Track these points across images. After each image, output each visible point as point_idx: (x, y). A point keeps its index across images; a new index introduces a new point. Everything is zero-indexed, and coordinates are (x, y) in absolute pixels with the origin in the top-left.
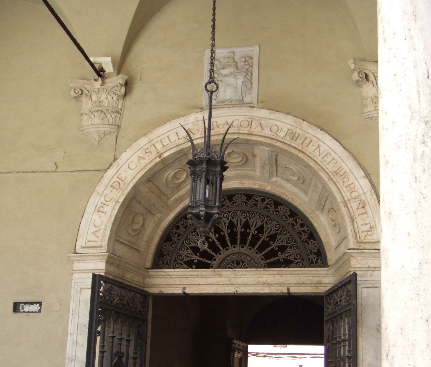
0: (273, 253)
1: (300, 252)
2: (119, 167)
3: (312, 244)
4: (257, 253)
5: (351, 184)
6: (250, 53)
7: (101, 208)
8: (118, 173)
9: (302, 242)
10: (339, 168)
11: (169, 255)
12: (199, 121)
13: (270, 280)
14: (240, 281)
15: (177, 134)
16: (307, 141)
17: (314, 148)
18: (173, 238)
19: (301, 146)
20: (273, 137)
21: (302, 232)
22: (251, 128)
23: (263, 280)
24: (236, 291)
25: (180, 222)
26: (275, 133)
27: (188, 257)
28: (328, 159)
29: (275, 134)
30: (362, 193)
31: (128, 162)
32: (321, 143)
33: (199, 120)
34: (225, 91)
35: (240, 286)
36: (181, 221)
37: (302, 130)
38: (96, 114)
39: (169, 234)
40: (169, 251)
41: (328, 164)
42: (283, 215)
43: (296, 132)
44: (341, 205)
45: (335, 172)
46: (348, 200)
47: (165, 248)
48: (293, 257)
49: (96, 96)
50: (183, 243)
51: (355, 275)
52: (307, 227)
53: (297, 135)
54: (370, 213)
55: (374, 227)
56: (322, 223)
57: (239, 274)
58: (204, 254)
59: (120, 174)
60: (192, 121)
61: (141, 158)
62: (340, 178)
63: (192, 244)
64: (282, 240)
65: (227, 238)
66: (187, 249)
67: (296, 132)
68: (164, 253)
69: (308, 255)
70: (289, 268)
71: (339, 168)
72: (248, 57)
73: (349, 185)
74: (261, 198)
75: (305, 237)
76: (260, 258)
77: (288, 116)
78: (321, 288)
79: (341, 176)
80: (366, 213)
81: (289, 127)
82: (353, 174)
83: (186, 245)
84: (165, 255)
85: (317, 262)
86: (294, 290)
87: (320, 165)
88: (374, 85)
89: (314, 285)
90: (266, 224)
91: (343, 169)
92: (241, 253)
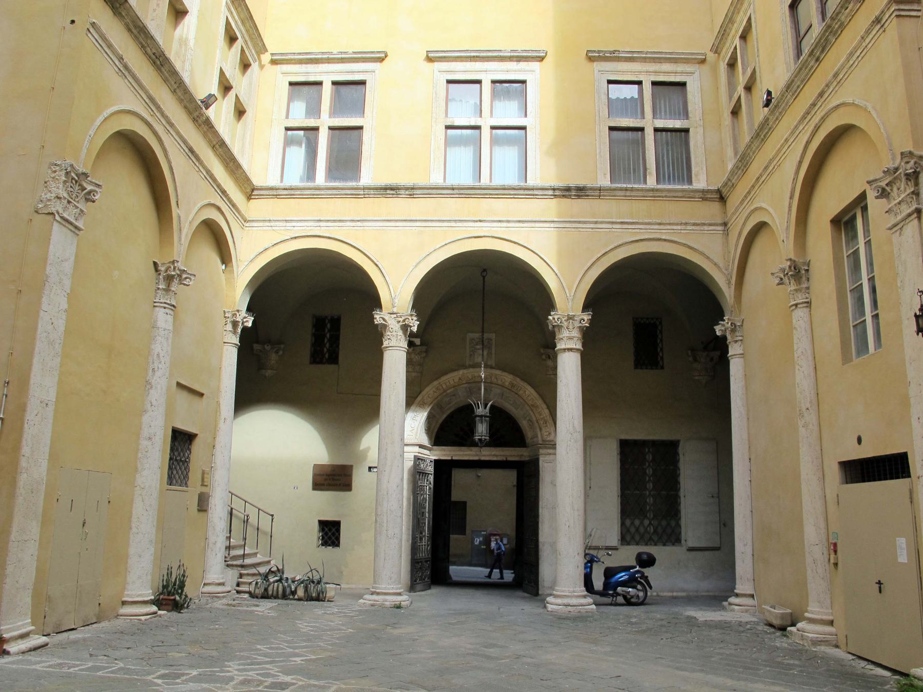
13: (497, 453)
56: (524, 424)
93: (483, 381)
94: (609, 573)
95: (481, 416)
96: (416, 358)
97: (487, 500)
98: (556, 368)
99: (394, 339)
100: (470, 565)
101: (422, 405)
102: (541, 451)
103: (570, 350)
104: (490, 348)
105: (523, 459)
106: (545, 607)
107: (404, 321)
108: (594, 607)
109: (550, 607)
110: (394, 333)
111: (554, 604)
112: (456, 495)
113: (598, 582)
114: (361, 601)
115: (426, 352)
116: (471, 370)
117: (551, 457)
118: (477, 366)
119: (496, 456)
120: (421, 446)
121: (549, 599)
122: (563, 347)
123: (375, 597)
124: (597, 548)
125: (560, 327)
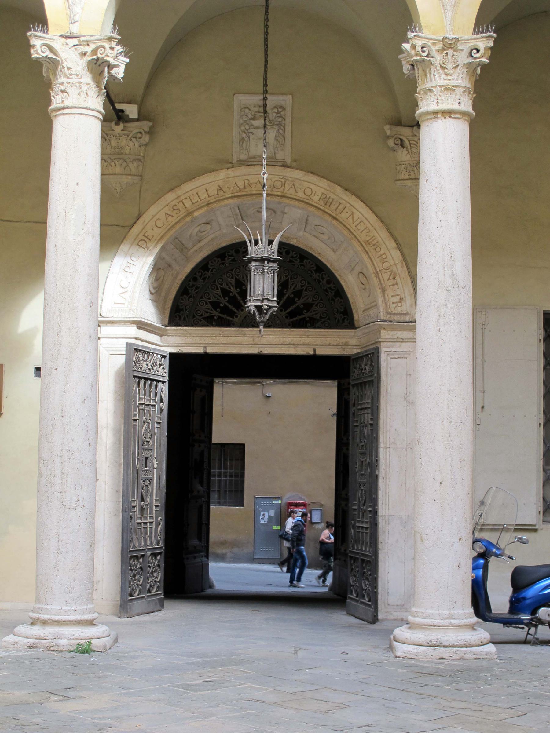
2: (145, 223)
6: (283, 103)
7: (128, 268)
8: (144, 231)
9: (329, 299)
13: (296, 340)
14: (264, 340)
16: (341, 207)
17: (348, 215)
18: (190, 291)
19: (335, 212)
20: (307, 201)
23: (288, 340)
27: (207, 312)
28: (361, 227)
29: (308, 198)
31: (155, 219)
32: (355, 211)
34: (256, 145)
42: (309, 270)
44: (373, 275)
45: (367, 241)
52: (334, 284)
53: (331, 200)
56: (350, 283)
58: (225, 310)
60: (222, 177)
62: (373, 247)
66: (207, 304)
68: (181, 308)
69: (335, 314)
74: (285, 250)
77: (322, 179)
79: (373, 245)
80: (397, 284)
81: (323, 191)
84: (182, 310)
86: (321, 352)
87: (354, 234)
88: (408, 152)
89: (340, 347)
90: (291, 279)
91: (375, 239)
93: (267, 204)
94: (521, 580)
95: (262, 260)
96: (130, 146)
97: (277, 432)
98: (417, 165)
99: (73, 91)
100: (252, 560)
101: (143, 241)
102: (384, 335)
103: (448, 113)
104: (281, 126)
105: (346, 352)
106: (391, 648)
107: (94, 52)
108: (491, 648)
109: (401, 649)
110: (74, 80)
111: (410, 643)
112: (222, 432)
113: (500, 597)
114: (11, 638)
115: (151, 132)
116: (243, 170)
117: (405, 346)
118: (253, 161)
120: (141, 325)
121: (401, 632)
122: (433, 107)
123: (38, 630)
124: (495, 528)
125: (425, 64)
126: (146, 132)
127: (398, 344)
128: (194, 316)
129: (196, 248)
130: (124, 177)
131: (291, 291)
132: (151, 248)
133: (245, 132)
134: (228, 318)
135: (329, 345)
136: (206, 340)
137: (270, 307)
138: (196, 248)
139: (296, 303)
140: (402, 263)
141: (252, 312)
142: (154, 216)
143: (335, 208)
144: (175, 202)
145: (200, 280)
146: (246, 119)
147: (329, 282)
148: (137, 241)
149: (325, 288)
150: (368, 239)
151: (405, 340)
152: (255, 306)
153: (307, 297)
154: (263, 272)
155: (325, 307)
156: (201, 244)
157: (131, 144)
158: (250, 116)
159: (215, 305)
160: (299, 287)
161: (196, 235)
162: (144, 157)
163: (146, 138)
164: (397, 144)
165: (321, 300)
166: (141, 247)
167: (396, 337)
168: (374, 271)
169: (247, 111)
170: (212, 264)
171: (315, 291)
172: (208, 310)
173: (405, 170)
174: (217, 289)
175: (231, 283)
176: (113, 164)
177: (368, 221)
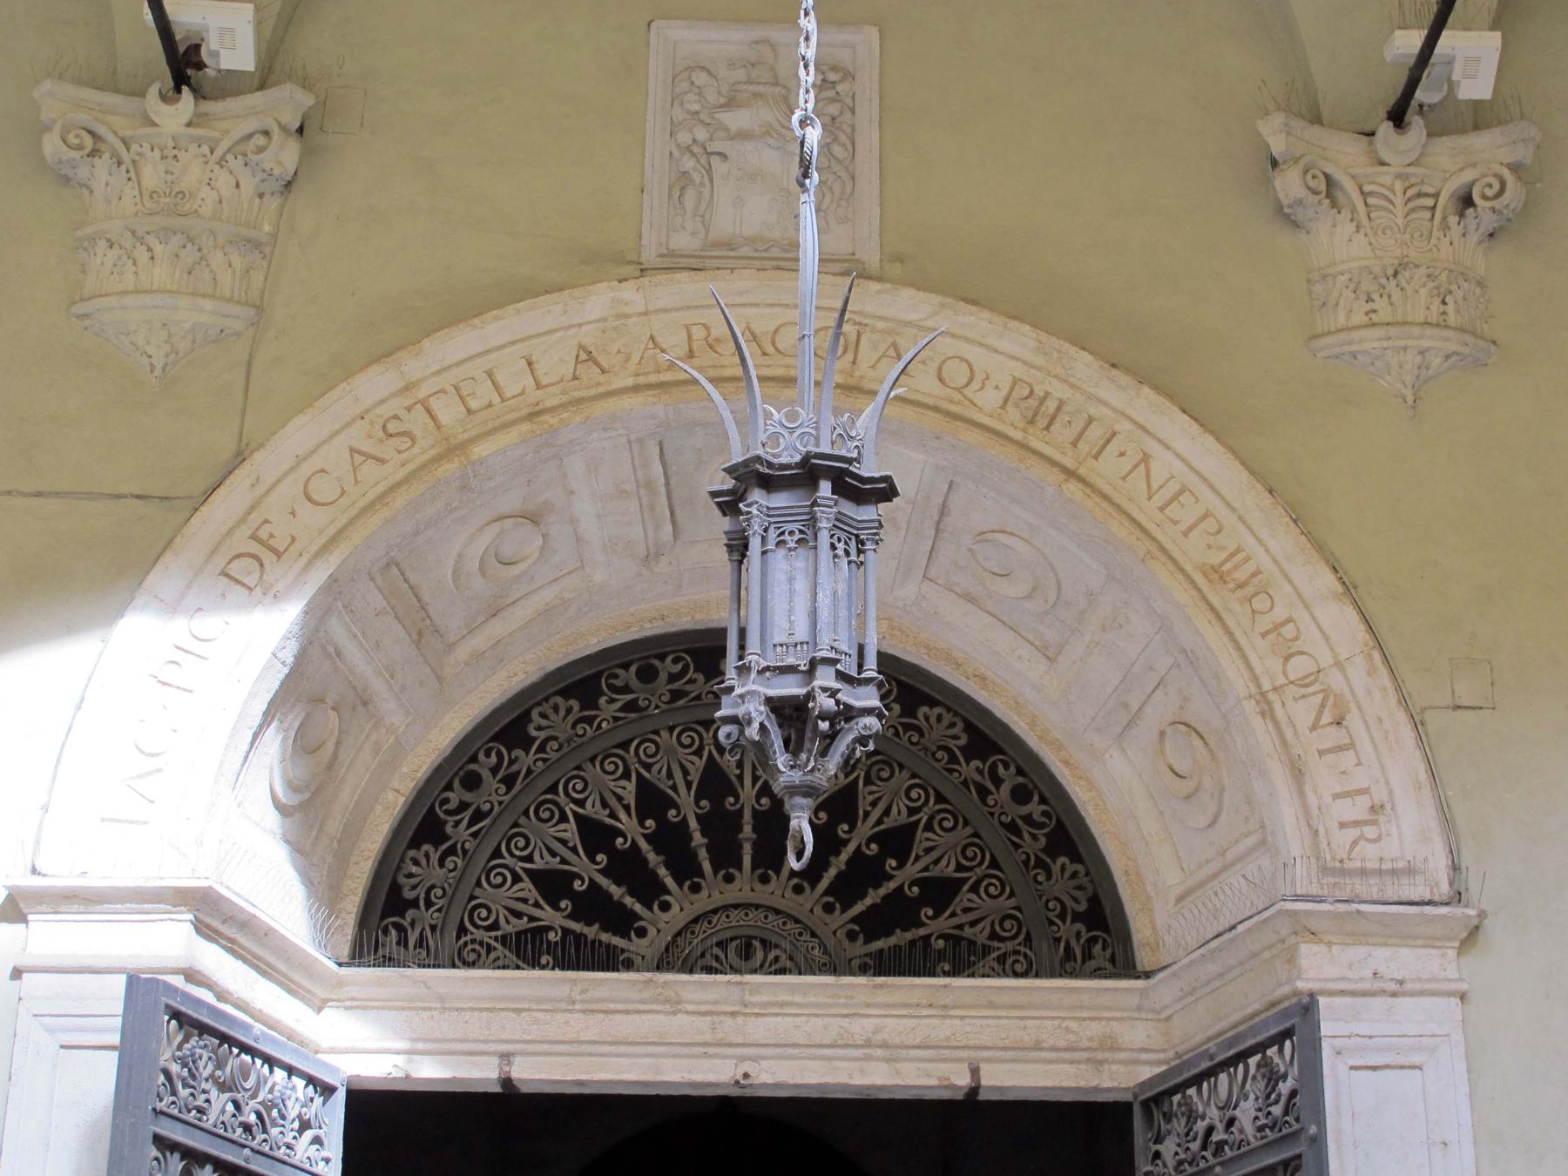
0: (899, 912)
1: (1018, 908)
2: (261, 489)
3: (1067, 875)
4: (829, 909)
5: (1283, 624)
8: (256, 519)
10: (1233, 555)
11: (429, 904)
12: (628, 316)
13: (893, 1028)
14: (759, 1029)
15: (530, 364)
16: (1096, 432)
17: (1126, 463)
18: (449, 829)
21: (1020, 822)
22: (854, 362)
23: (861, 1028)
24: (746, 1076)
25: (481, 756)
26: (959, 390)
27: (518, 915)
28: (1186, 513)
29: (957, 396)
30: (1331, 662)
31: (306, 469)
33: (628, 310)
35: (763, 1051)
36: (488, 755)
37: (1073, 386)
38: (158, 248)
39: (431, 809)
40: (433, 887)
41: (1186, 534)
42: (940, 748)
43: (1047, 394)
44: (1250, 706)
46: (1275, 689)
47: (414, 869)
48: (987, 932)
49: (161, 167)
50: (497, 854)
51: (1307, 1008)
52: (1043, 800)
53: (1051, 406)
54: (1365, 746)
55: (1388, 806)
57: (756, 999)
58: (593, 906)
59: (266, 521)
61: (367, 456)
62: (1239, 593)
63: (537, 857)
64: (938, 852)
65: (698, 839)
66: (517, 879)
67: (1047, 394)
68: (408, 894)
69: (1051, 923)
70: (972, 975)
71: (1233, 555)
72: (834, 69)
73: (1278, 626)
75: (1034, 844)
76: (845, 930)
77: (1013, 324)
78: (1114, 1068)
79: (1240, 586)
80: (1351, 746)
81: (1018, 369)
82: (1290, 581)
83: (508, 860)
84: (414, 904)
85: (1088, 955)
87: (1154, 539)
89: (1085, 1055)
90: (868, 781)
91: (1247, 559)
92: (757, 907)
116: (683, 287)
119: (892, 1050)
120: (213, 915)
126: (283, 128)
127: (1378, 1003)
128: (462, 930)
129: (478, 642)
130: (184, 302)
131: (865, 829)
132: (280, 586)
133: (691, 152)
134: (605, 937)
135: (1037, 1047)
136: (512, 1028)
137: (849, 713)
138: (478, 642)
139: (890, 878)
140: (1369, 656)
141: (753, 732)
142: (300, 460)
143: (1072, 439)
144: (394, 406)
145: (491, 783)
146: (696, 107)
147: (1021, 795)
148: (220, 561)
149: (1006, 819)
150: (1215, 558)
151: (1409, 986)
152: (769, 701)
153: (934, 855)
154: (808, 539)
155: (1012, 894)
156: (497, 628)
157: (224, 180)
158: (712, 98)
159: (552, 885)
160: (899, 816)
161: (482, 570)
162: (274, 236)
163: (286, 155)
164: (1315, 192)
165: (994, 864)
166: (238, 582)
167: (1368, 973)
168: (1254, 690)
169: (701, 78)
170: (544, 723)
171: (968, 830)
172: (520, 907)
173: (1349, 294)
174: (564, 818)
175: (620, 798)
176: (142, 254)
177: (1212, 488)
